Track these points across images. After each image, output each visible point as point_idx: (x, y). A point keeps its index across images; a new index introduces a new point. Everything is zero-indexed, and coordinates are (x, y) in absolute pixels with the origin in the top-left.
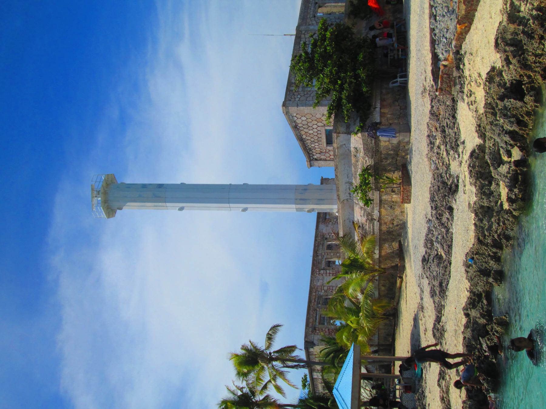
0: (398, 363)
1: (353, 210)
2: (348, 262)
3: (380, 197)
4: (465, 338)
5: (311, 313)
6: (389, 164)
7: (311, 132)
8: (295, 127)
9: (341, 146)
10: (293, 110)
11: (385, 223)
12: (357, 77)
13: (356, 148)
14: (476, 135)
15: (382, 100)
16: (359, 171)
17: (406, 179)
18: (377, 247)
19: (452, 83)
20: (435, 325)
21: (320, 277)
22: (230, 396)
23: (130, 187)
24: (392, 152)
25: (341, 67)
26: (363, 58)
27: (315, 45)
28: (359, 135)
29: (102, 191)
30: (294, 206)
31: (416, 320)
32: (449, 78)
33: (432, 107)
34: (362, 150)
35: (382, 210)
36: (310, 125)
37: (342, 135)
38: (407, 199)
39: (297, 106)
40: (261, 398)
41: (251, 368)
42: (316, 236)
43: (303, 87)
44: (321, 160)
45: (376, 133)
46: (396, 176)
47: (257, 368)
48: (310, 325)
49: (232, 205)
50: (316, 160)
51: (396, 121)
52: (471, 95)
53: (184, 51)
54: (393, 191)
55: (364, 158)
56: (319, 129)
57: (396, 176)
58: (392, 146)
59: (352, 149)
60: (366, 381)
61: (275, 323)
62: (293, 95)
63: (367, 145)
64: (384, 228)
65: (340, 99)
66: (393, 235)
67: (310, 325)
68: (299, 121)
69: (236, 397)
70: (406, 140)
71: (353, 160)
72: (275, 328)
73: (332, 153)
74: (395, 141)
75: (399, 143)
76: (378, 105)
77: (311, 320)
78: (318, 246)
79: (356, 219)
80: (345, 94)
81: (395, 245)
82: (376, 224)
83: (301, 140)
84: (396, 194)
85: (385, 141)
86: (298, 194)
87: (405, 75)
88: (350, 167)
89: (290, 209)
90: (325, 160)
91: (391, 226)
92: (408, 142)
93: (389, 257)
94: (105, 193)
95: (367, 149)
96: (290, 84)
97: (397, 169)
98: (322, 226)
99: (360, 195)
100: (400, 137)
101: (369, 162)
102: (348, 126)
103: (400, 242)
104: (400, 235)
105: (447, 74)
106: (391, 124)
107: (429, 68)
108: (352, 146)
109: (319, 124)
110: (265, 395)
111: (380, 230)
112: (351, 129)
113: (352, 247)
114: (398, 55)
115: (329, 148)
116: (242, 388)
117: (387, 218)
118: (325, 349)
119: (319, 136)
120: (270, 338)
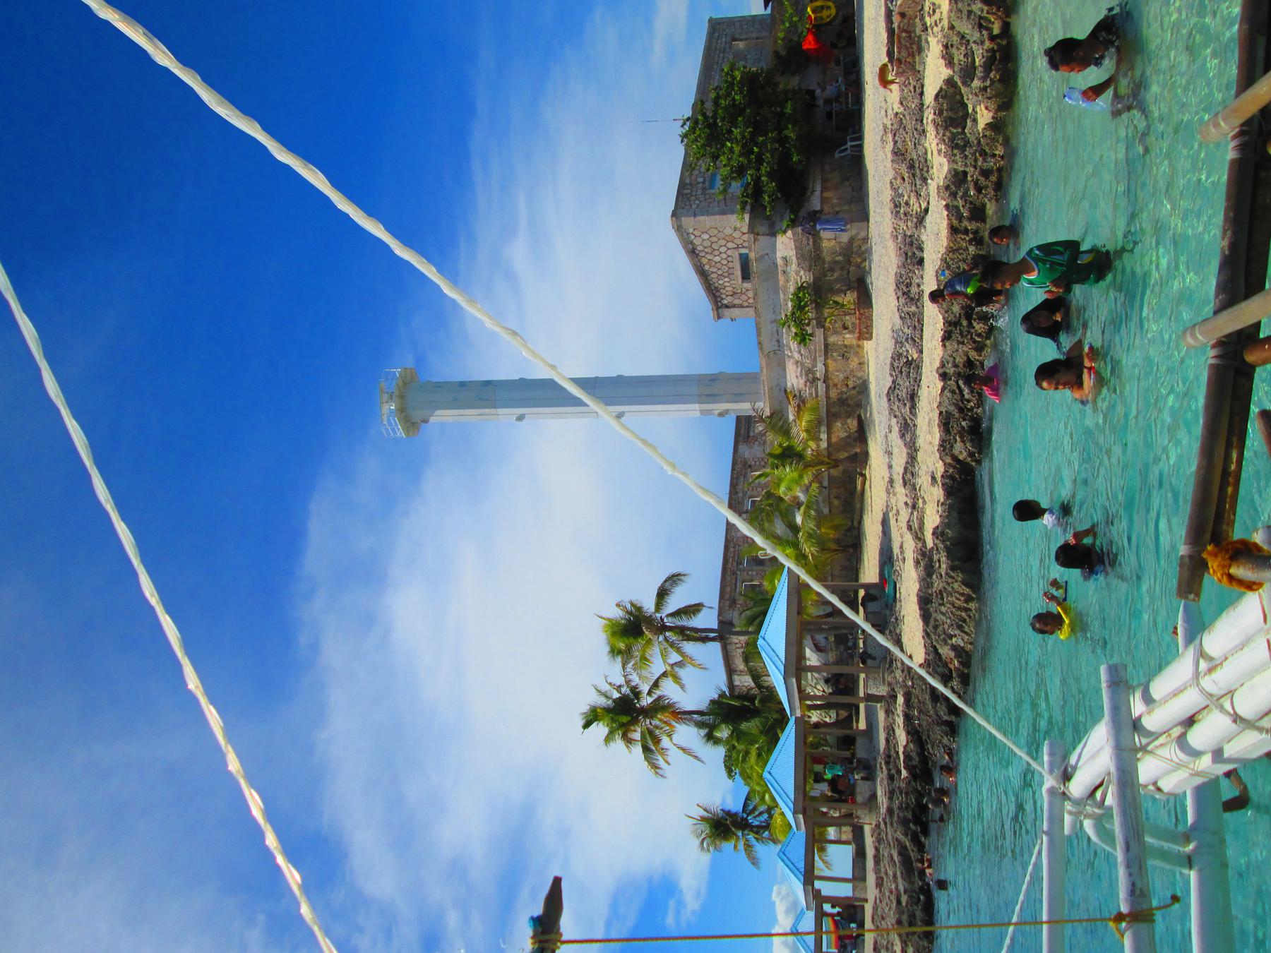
0: (862, 593)
1: (784, 370)
2: (778, 451)
3: (825, 339)
4: (941, 413)
5: (728, 578)
6: (837, 280)
7: (717, 259)
8: (693, 252)
9: (762, 257)
10: (688, 222)
11: (835, 385)
12: (782, 140)
13: (785, 259)
14: (942, 62)
16: (792, 290)
17: (865, 299)
18: (824, 429)
19: (915, 47)
20: (906, 469)
22: (602, 701)
23: (439, 386)
24: (840, 258)
25: (758, 128)
26: (794, 109)
27: (716, 102)
28: (789, 233)
29: (397, 393)
30: (697, 406)
31: (885, 522)
32: (910, 37)
33: (895, 142)
34: (794, 258)
37: (762, 238)
38: (865, 332)
39: (695, 215)
40: (650, 700)
41: (631, 640)
42: (734, 463)
43: (704, 189)
44: (734, 306)
45: (815, 226)
46: (849, 298)
47: (641, 641)
48: (727, 596)
50: (727, 306)
51: (846, 208)
52: (934, 11)
53: (518, 253)
54: (845, 328)
55: (797, 273)
56: (729, 253)
57: (849, 298)
58: (841, 248)
59: (779, 262)
60: (816, 675)
61: (675, 571)
62: (690, 198)
63: (801, 249)
64: (834, 394)
65: (757, 180)
66: (849, 406)
67: (727, 596)
69: (610, 702)
70: (862, 235)
71: (781, 278)
72: (674, 579)
73: (751, 294)
74: (845, 238)
75: (851, 241)
76: (818, 188)
77: (728, 589)
78: (738, 478)
79: (789, 385)
80: (765, 168)
81: (853, 423)
82: (821, 386)
83: (702, 274)
84: (850, 332)
85: (830, 239)
87: (860, 138)
88: (777, 293)
89: (693, 410)
90: (741, 306)
91: (844, 389)
93: (845, 443)
94: (402, 396)
95: (801, 257)
96: (682, 185)
98: (743, 448)
99: (794, 330)
100: (853, 230)
101: (806, 277)
102: (772, 225)
103: (859, 416)
104: (859, 405)
105: (906, 31)
106: (838, 213)
107: (885, 50)
108: (779, 255)
109: (730, 245)
110: (655, 696)
111: (828, 397)
112: (777, 228)
113: (786, 431)
114: (847, 104)
115: (746, 285)
116: (620, 686)
117: (838, 377)
119: (730, 265)
120: (662, 594)
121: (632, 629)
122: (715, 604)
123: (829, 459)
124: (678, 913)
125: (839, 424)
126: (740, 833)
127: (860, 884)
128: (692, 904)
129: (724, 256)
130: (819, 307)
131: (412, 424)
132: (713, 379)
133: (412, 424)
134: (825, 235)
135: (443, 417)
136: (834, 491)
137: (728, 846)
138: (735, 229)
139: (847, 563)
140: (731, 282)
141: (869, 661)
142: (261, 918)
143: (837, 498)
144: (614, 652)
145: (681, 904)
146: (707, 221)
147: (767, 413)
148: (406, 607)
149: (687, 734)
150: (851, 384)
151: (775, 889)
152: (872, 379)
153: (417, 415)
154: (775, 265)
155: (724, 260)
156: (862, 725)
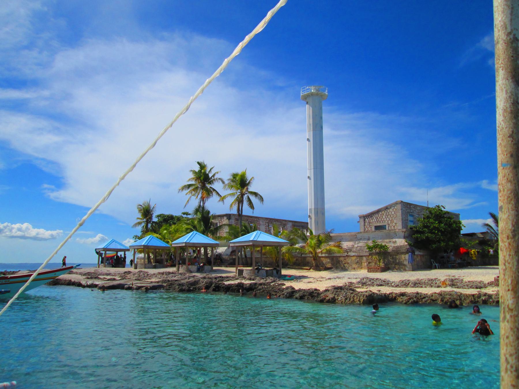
2: (320, 239)
7: (384, 217)
8: (386, 208)
9: (396, 234)
10: (399, 207)
11: (345, 259)
12: (439, 241)
15: (423, 256)
21: (264, 223)
23: (321, 109)
24: (397, 261)
30: (313, 207)
35: (355, 257)
36: (389, 216)
42: (285, 221)
43: (409, 212)
44: (365, 223)
49: (312, 170)
50: (364, 220)
54: (369, 263)
56: (386, 221)
57: (382, 265)
59: (394, 240)
64: (342, 259)
66: (337, 264)
68: (391, 210)
70: (407, 269)
71: (388, 240)
72: (261, 199)
74: (406, 263)
75: (405, 265)
76: (421, 253)
78: (280, 222)
79: (343, 243)
81: (329, 265)
83: (378, 212)
85: (405, 258)
86: (320, 209)
87: (439, 268)
88: (381, 239)
90: (364, 225)
92: (405, 270)
94: (317, 95)
95: (398, 247)
97: (386, 265)
100: (409, 266)
101: (390, 249)
104: (337, 268)
108: (397, 240)
109: (389, 222)
111: (340, 257)
117: (349, 260)
118: (494, 230)
119: (381, 222)
120: (256, 194)
121: (241, 182)
122: (254, 215)
123: (316, 258)
124: (49, 189)
125: (329, 260)
126: (145, 220)
127: (143, 266)
128: (53, 195)
129: (385, 219)
130: (378, 254)
131: (306, 98)
132: (323, 214)
133: (306, 98)
134: (407, 256)
135: (308, 110)
136: (300, 259)
137: (140, 215)
138: (396, 224)
139: (268, 263)
140: (374, 222)
141: (257, 271)
142: (46, 9)
143: (297, 260)
144: (235, 176)
145: (53, 190)
146: (399, 214)
147: (331, 235)
148: (178, 79)
149: (195, 202)
150: (346, 265)
151: (62, 231)
152: (348, 272)
153: (310, 100)
154: (393, 238)
155: (383, 220)
156: (214, 268)
